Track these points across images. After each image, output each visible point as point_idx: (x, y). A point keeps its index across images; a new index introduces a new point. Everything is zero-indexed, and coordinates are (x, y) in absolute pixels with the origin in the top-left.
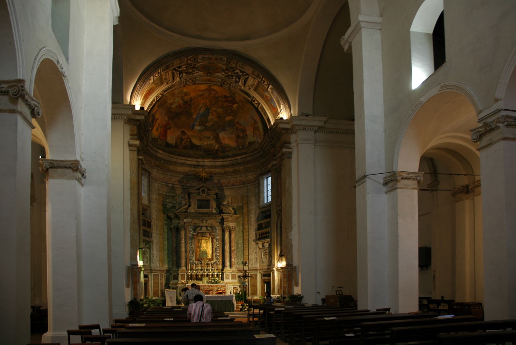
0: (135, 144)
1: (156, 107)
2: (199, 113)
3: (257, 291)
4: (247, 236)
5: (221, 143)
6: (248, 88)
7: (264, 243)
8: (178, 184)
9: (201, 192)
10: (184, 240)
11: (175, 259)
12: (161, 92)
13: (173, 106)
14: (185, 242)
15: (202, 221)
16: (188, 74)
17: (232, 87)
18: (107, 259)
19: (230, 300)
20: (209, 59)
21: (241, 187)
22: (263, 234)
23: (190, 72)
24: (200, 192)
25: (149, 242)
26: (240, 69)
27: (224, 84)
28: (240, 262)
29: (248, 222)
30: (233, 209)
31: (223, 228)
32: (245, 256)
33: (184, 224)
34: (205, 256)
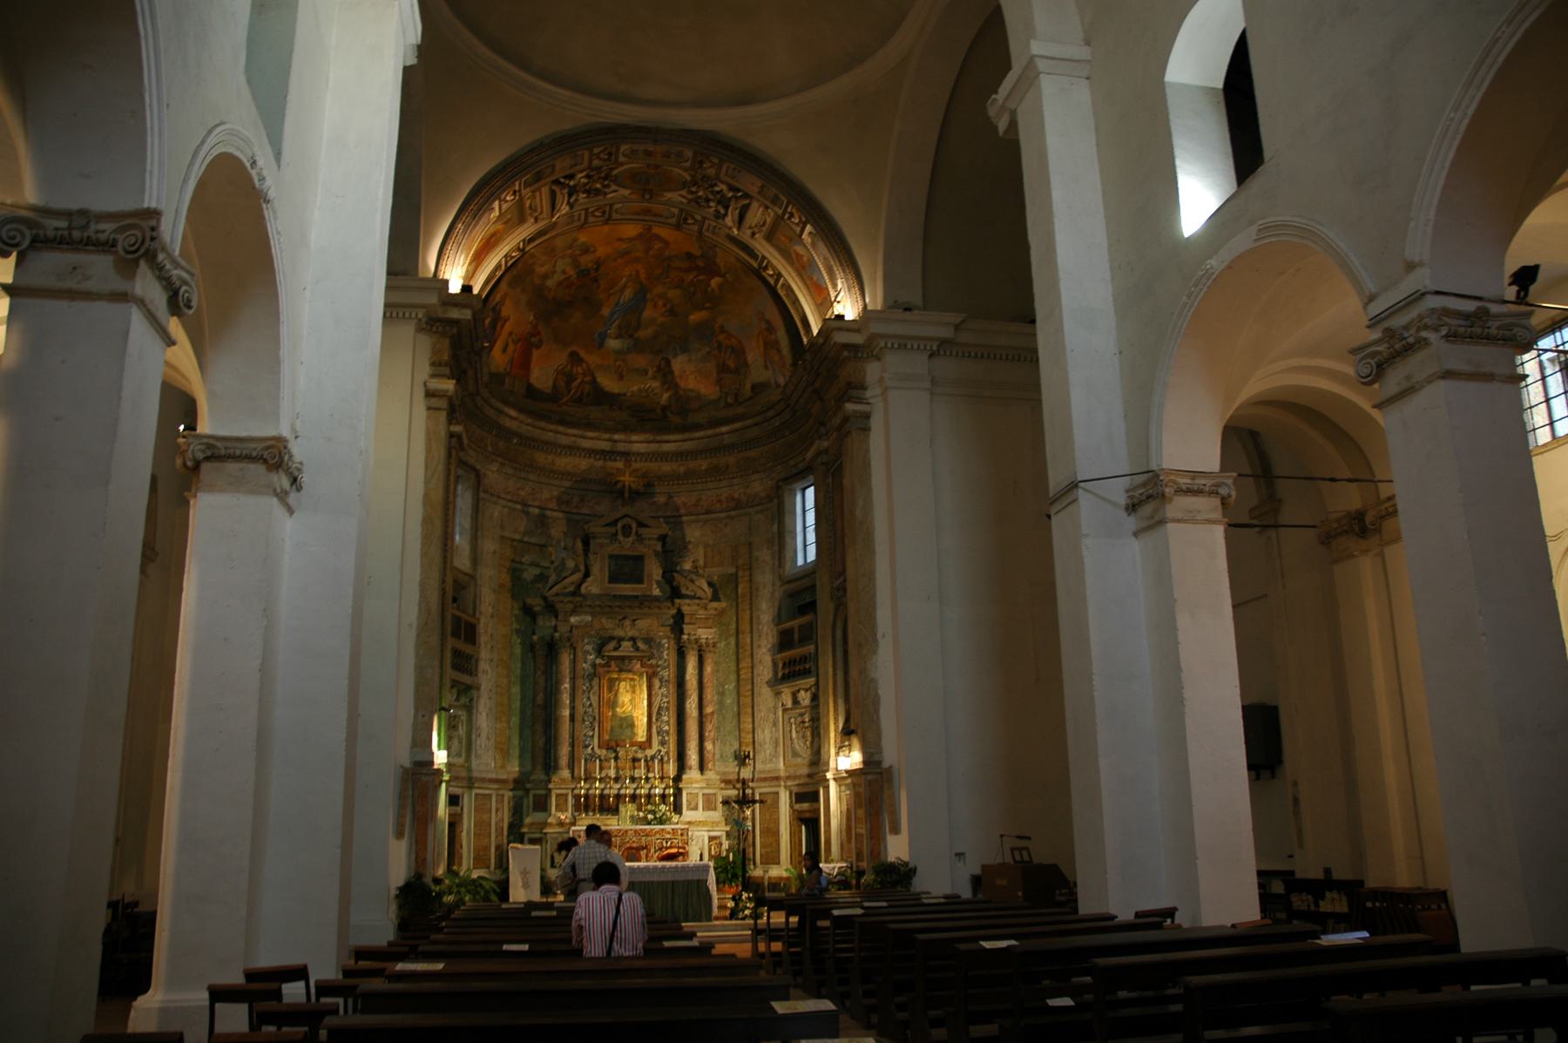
0: (442, 391)
1: (503, 286)
3: (778, 851)
4: (750, 670)
5: (677, 386)
6: (749, 232)
7: (799, 691)
8: (556, 508)
9: (619, 532)
10: (568, 680)
11: (541, 742)
12: (519, 243)
13: (550, 283)
15: (620, 621)
19: (698, 881)
20: (649, 154)
21: (732, 518)
23: (597, 189)
26: (729, 180)
27: (686, 223)
28: (729, 755)
30: (710, 584)
31: (681, 645)
32: (743, 734)
33: (571, 631)
34: (628, 732)
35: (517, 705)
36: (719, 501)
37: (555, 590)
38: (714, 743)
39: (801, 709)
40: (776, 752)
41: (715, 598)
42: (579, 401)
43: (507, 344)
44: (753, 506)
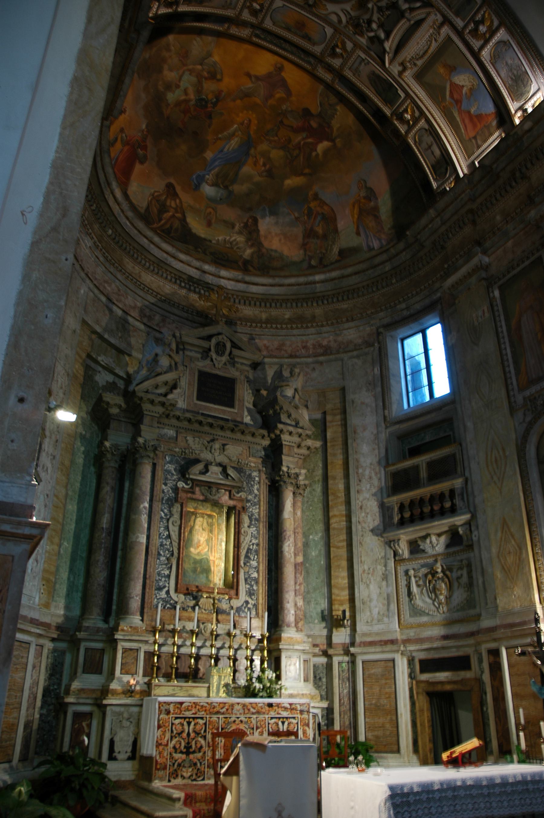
2: (222, 151)
13: (171, 97)
21: (321, 363)
28: (314, 615)
32: (334, 591)
36: (305, 347)
44: (346, 352)
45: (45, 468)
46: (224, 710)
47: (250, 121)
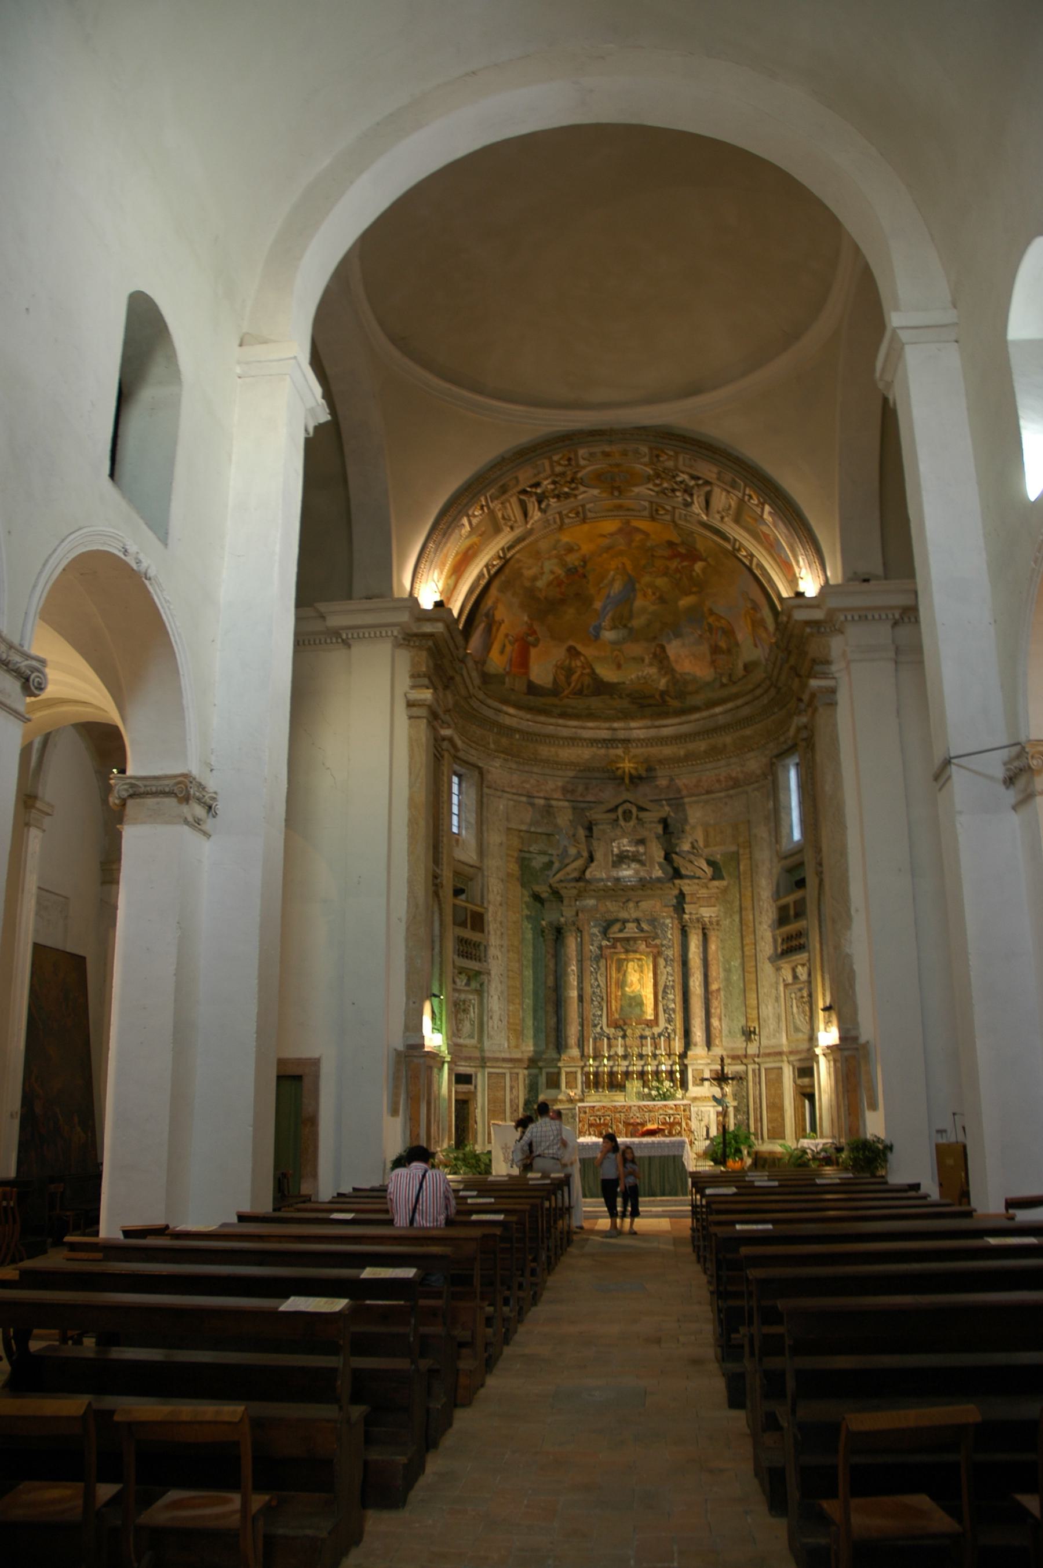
0: (421, 700)
1: (494, 591)
3: (783, 1126)
4: (753, 947)
5: (673, 670)
6: (718, 517)
7: (796, 966)
8: (561, 797)
9: (621, 817)
10: (574, 963)
11: (553, 1022)
12: (498, 552)
13: (540, 584)
14: (577, 968)
15: (624, 903)
16: (562, 499)
17: (680, 519)
18: (255, 1036)
19: (674, 1157)
20: (607, 455)
21: (731, 797)
22: (792, 936)
23: (566, 493)
24: (618, 817)
25: (478, 973)
26: (688, 470)
27: (658, 514)
28: (737, 1030)
29: (753, 900)
30: (711, 863)
31: (684, 924)
32: (749, 1011)
33: (577, 915)
34: (637, 1010)
35: (530, 987)
36: (719, 781)
37: (559, 876)
38: (720, 1020)
39: (800, 983)
40: (779, 1027)
41: (717, 875)
42: (579, 693)
43: (504, 646)
45: (495, 957)
46: (625, 1110)
47: (623, 564)
